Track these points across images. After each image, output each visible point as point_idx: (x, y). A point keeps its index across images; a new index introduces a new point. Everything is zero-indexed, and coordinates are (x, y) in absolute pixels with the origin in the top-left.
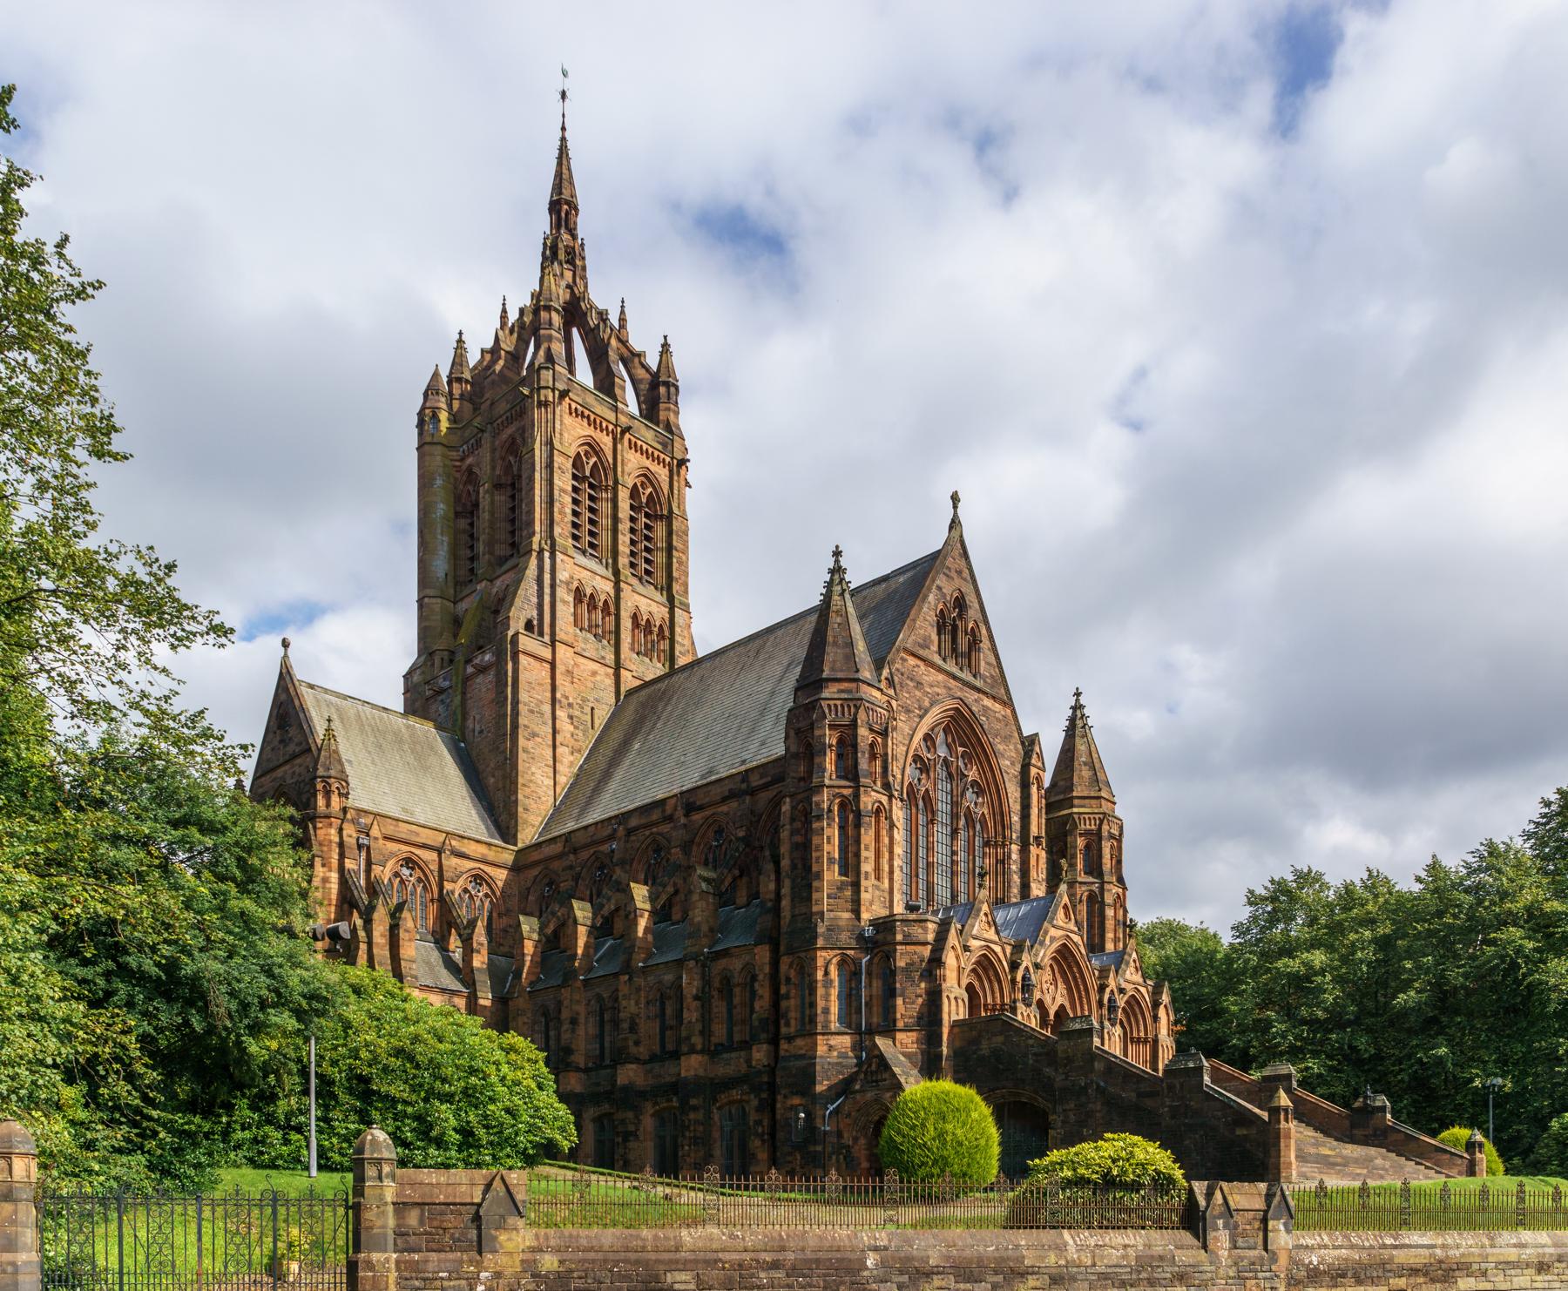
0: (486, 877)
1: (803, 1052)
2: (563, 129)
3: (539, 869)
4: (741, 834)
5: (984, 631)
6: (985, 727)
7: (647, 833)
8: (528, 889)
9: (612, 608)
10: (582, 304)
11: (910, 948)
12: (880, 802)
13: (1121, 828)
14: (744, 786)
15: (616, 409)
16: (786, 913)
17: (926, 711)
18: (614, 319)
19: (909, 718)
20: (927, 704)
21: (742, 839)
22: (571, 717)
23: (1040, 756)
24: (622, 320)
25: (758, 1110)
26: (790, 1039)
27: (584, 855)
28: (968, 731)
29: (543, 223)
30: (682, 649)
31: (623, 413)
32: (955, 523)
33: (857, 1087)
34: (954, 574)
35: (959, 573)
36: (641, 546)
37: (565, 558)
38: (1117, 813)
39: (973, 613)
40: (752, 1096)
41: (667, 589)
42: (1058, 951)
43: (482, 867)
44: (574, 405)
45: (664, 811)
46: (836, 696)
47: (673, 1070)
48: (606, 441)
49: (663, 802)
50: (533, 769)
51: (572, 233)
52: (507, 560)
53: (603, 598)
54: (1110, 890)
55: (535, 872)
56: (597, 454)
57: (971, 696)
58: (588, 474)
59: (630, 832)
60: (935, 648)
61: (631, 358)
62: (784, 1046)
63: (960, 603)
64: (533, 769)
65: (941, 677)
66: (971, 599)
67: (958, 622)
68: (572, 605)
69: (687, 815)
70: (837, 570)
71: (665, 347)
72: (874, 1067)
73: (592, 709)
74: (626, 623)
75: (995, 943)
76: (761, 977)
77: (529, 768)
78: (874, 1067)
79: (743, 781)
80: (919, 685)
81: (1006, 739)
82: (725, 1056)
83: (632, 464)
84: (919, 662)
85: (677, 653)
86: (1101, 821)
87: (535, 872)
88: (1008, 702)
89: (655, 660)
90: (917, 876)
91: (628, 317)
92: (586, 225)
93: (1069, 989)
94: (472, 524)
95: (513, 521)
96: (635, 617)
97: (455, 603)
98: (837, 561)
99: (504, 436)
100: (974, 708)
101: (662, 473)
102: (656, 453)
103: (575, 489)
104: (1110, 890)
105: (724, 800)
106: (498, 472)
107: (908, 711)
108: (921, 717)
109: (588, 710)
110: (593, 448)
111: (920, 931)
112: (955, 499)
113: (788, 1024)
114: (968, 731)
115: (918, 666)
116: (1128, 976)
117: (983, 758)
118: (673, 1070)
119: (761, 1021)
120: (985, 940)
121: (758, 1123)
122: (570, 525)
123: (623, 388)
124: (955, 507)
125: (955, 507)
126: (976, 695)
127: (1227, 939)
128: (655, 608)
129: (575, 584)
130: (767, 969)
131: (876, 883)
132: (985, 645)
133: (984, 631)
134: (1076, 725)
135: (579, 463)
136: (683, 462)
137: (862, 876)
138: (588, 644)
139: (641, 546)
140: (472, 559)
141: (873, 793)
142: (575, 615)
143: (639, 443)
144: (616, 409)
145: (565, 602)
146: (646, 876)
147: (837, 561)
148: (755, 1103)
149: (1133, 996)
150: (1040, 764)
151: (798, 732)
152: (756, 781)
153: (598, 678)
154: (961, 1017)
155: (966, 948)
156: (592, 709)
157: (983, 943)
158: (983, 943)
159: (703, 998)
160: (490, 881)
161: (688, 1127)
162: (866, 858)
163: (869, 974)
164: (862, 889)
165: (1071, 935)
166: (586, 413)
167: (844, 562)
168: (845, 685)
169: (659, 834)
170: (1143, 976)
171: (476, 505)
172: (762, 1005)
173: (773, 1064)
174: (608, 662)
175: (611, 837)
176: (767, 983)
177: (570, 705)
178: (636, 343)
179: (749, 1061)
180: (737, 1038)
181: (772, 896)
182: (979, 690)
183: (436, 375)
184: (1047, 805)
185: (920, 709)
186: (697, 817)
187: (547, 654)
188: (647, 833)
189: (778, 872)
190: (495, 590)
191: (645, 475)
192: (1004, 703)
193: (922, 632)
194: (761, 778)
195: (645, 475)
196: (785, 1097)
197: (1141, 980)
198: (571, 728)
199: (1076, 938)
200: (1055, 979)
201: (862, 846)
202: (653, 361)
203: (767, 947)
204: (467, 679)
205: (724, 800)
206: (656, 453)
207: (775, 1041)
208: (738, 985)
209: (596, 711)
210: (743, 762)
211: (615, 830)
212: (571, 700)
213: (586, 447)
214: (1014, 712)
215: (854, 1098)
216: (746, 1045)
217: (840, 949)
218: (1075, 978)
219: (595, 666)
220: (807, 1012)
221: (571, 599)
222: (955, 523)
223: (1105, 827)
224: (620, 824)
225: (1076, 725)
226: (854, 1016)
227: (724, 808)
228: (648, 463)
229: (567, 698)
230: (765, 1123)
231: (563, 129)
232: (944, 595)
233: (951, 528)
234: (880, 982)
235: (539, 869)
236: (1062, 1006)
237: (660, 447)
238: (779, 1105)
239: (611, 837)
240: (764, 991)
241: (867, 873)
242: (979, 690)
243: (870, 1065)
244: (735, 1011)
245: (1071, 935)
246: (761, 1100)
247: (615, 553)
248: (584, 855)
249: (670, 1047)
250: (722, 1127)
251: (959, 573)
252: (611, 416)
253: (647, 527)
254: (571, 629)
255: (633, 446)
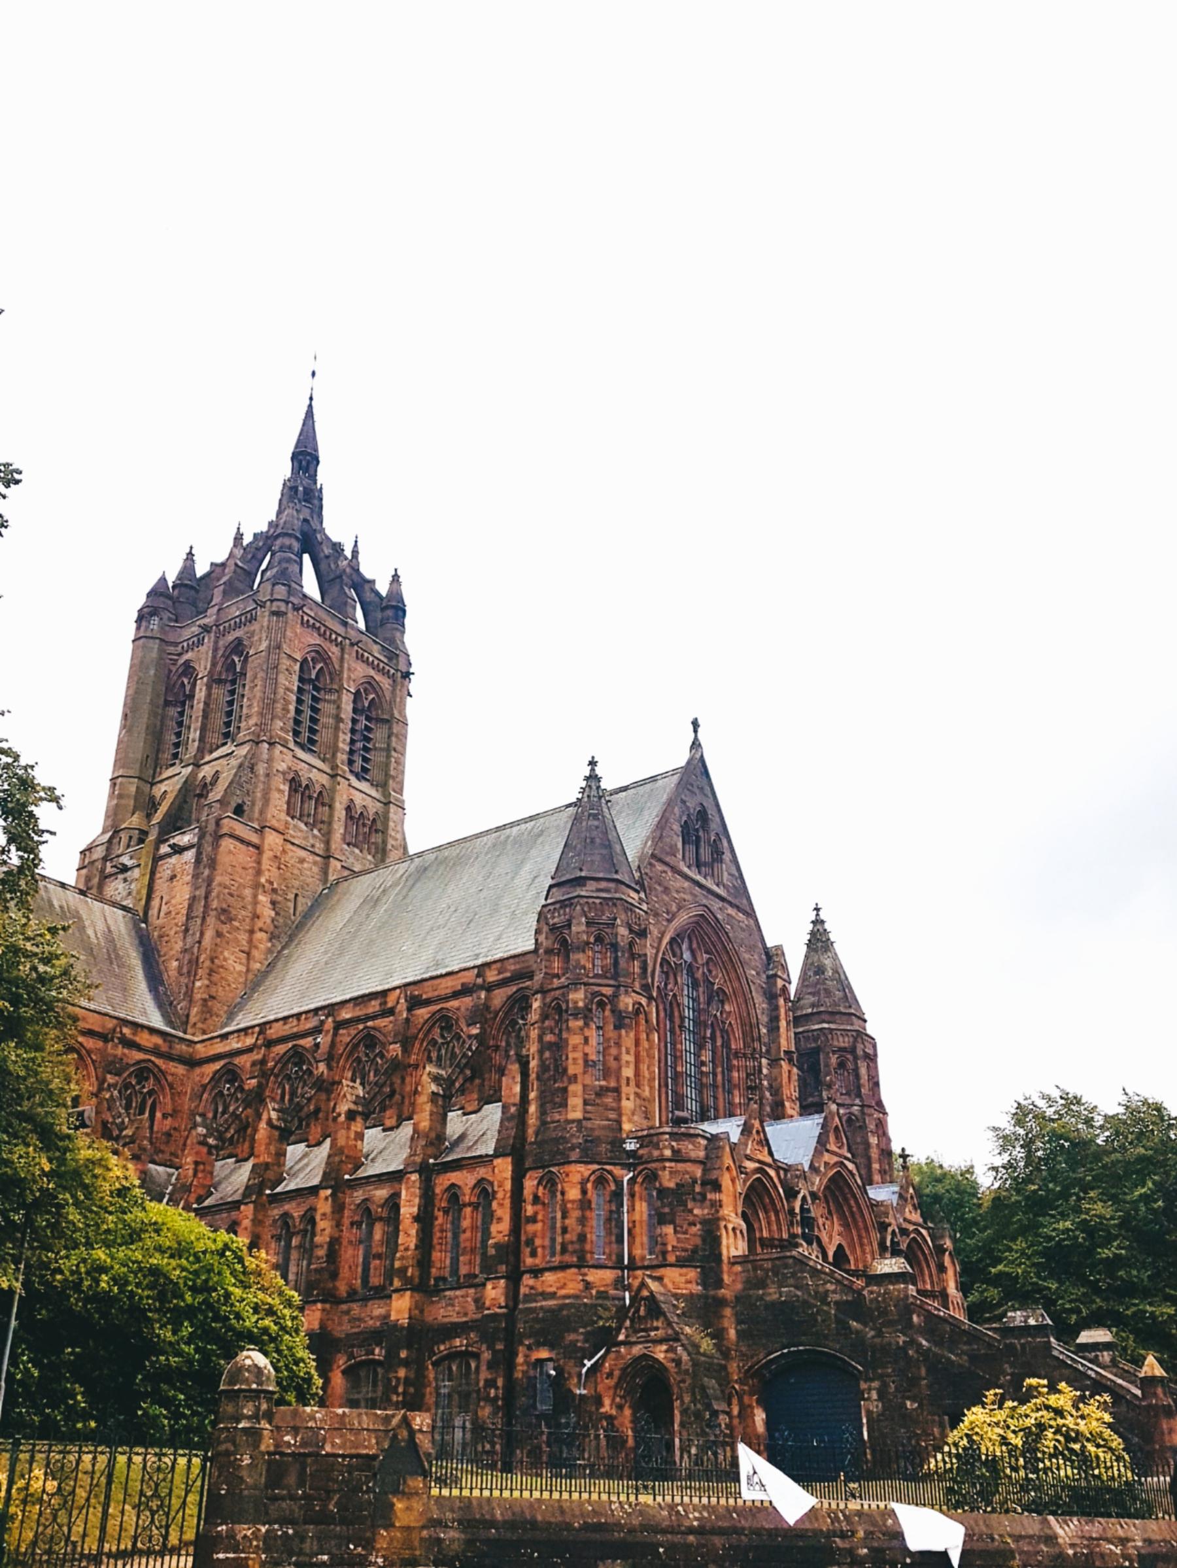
0: (156, 1070)
1: (553, 1289)
2: (311, 399)
3: (222, 1063)
4: (475, 1031)
5: (725, 844)
6: (731, 935)
7: (361, 1027)
8: (204, 1087)
9: (324, 799)
10: (319, 536)
11: (680, 1166)
12: (640, 1004)
13: (875, 1046)
14: (480, 981)
15: (345, 624)
16: (532, 1120)
17: (674, 916)
18: (348, 553)
19: (658, 922)
20: (674, 908)
21: (476, 1036)
22: (273, 903)
23: (785, 968)
24: (355, 553)
25: (491, 1366)
26: (536, 1272)
27: (281, 1049)
28: (714, 938)
29: (285, 469)
30: (393, 843)
31: (353, 627)
32: (696, 745)
33: (621, 1337)
34: (697, 791)
35: (701, 789)
36: (359, 745)
37: (285, 750)
38: (869, 1032)
39: (714, 826)
40: (484, 1347)
41: (382, 786)
42: (831, 1179)
43: (153, 1058)
44: (306, 618)
45: (385, 1003)
46: (594, 895)
47: (378, 1311)
48: (334, 651)
49: (384, 993)
50: (226, 954)
51: (313, 478)
52: (218, 747)
53: (318, 789)
54: (871, 1115)
55: (217, 1066)
56: (324, 661)
57: (716, 905)
58: (313, 677)
59: (339, 1025)
60: (680, 856)
61: (362, 585)
62: (528, 1280)
63: (703, 815)
64: (226, 954)
65: (687, 884)
66: (711, 812)
67: (701, 833)
68: (286, 793)
69: (409, 1010)
70: (593, 778)
71: (396, 578)
72: (642, 1312)
73: (296, 895)
74: (340, 813)
75: (770, 1166)
76: (500, 1195)
77: (222, 953)
78: (642, 1312)
79: (478, 976)
80: (666, 890)
81: (751, 949)
82: (448, 1293)
83: (355, 673)
84: (666, 868)
85: (389, 847)
86: (855, 1039)
87: (217, 1066)
88: (750, 913)
89: (365, 851)
90: (667, 1086)
91: (360, 549)
92: (325, 475)
93: (846, 1225)
94: (181, 714)
95: (229, 714)
96: (348, 809)
97: (152, 784)
98: (593, 770)
99: (230, 638)
100: (719, 916)
101: (385, 683)
102: (382, 665)
103: (300, 690)
104: (871, 1115)
105: (456, 995)
106: (218, 668)
107: (656, 915)
108: (670, 921)
109: (291, 896)
110: (320, 655)
111: (691, 1147)
112: (695, 724)
113: (534, 1254)
114: (714, 938)
115: (665, 872)
116: (907, 1215)
117: (729, 967)
118: (378, 1311)
119: (497, 1246)
120: (759, 1162)
121: (490, 1383)
122: (291, 721)
123: (355, 608)
124: (695, 731)
125: (695, 731)
126: (721, 904)
127: (986, 1181)
128: (369, 802)
129: (292, 775)
130: (508, 1185)
131: (637, 1090)
132: (727, 856)
133: (725, 844)
134: (819, 940)
135: (305, 668)
136: (407, 675)
137: (624, 1082)
138: (299, 830)
139: (359, 745)
140: (177, 745)
141: (633, 994)
142: (288, 803)
143: (366, 654)
144: (345, 624)
145: (280, 791)
146: (354, 1075)
147: (593, 770)
148: (486, 1355)
149: (914, 1238)
150: (785, 976)
151: (553, 929)
152: (492, 976)
153: (306, 865)
154: (739, 1253)
155: (741, 1169)
156: (296, 895)
157: (757, 1165)
158: (757, 1165)
159: (424, 1219)
160: (159, 1075)
161: (396, 1387)
162: (627, 1062)
163: (632, 1195)
164: (624, 1096)
165: (846, 1162)
166: (318, 625)
167: (599, 771)
168: (603, 885)
169: (374, 1028)
170: (922, 1215)
171: (191, 696)
172: (500, 1230)
173: (511, 1304)
174: (317, 851)
175: (317, 1030)
176: (507, 1202)
177: (274, 891)
178: (367, 571)
179: (479, 1302)
180: (463, 1270)
181: (517, 1100)
182: (722, 899)
183: (163, 580)
184: (794, 1018)
185: (668, 913)
186: (423, 1013)
187: (254, 838)
188: (361, 1027)
189: (525, 1074)
190: (201, 776)
191: (369, 683)
192: (745, 913)
193: (668, 840)
194: (499, 973)
195: (369, 683)
196: (529, 1348)
197: (921, 1220)
198: (273, 914)
199: (851, 1166)
200: (830, 1212)
201: (624, 1049)
202: (383, 588)
203: (509, 1159)
204: (157, 859)
205: (456, 995)
206: (382, 665)
207: (514, 1279)
208: (470, 1204)
209: (300, 899)
210: (477, 956)
211: (322, 1022)
212: (275, 886)
213: (313, 654)
214: (756, 921)
215: (618, 1352)
216: (382, 1294)
217: (599, 1163)
218: (852, 1213)
219: (303, 854)
220: (559, 1239)
221: (286, 788)
222: (696, 745)
223: (860, 1046)
224: (327, 1016)
225: (819, 940)
226: (614, 1246)
227: (454, 1003)
228: (372, 673)
229: (271, 883)
230: (500, 1382)
231: (311, 399)
232: (688, 808)
233: (692, 748)
234: (644, 1204)
235: (222, 1063)
236: (840, 1246)
237: (385, 660)
238: (520, 1359)
239: (317, 1030)
240: (502, 1210)
241: (628, 1079)
242: (722, 899)
243: (638, 1311)
244: (463, 1237)
245: (846, 1162)
246: (495, 1352)
247: (335, 750)
248: (281, 1049)
249: (375, 1281)
250: (437, 1388)
251: (701, 789)
252: (340, 629)
253: (368, 729)
254: (283, 816)
255: (359, 657)
